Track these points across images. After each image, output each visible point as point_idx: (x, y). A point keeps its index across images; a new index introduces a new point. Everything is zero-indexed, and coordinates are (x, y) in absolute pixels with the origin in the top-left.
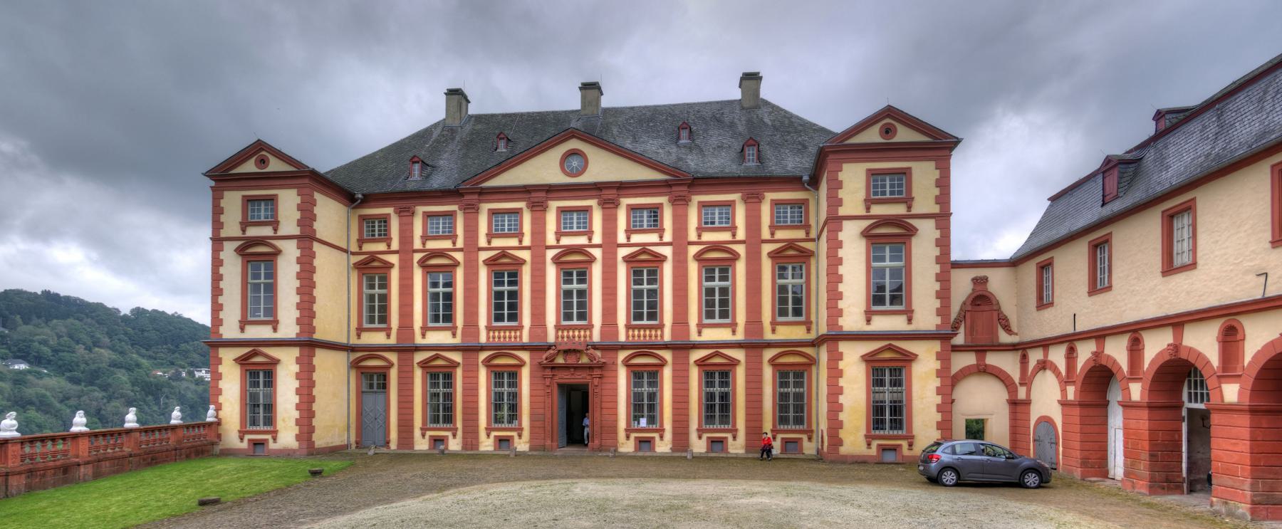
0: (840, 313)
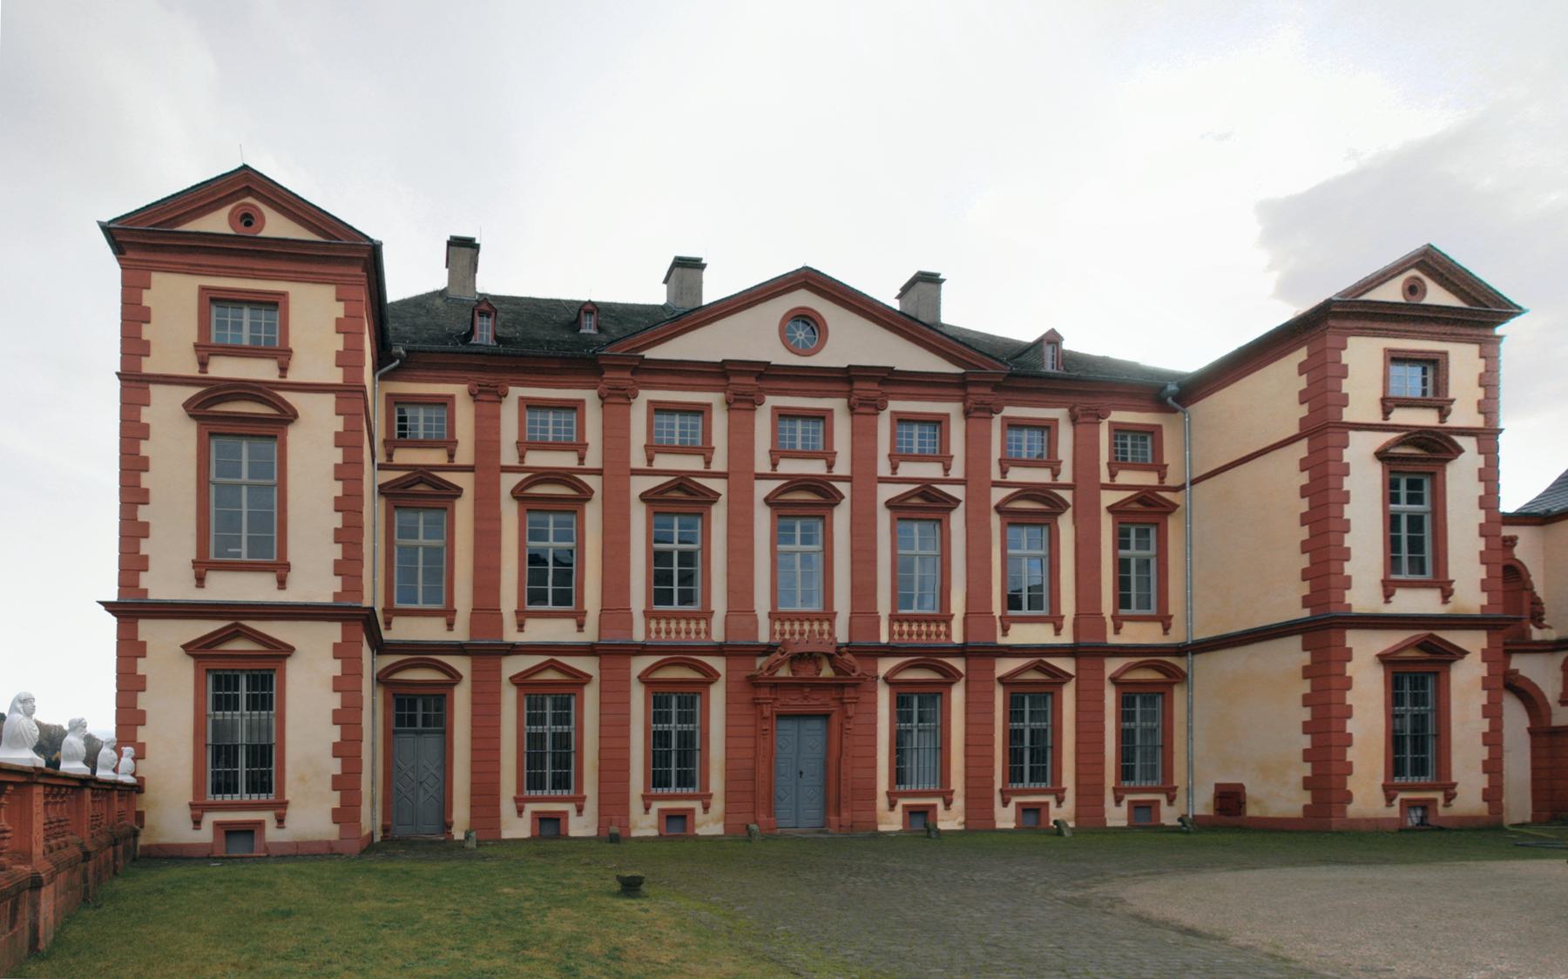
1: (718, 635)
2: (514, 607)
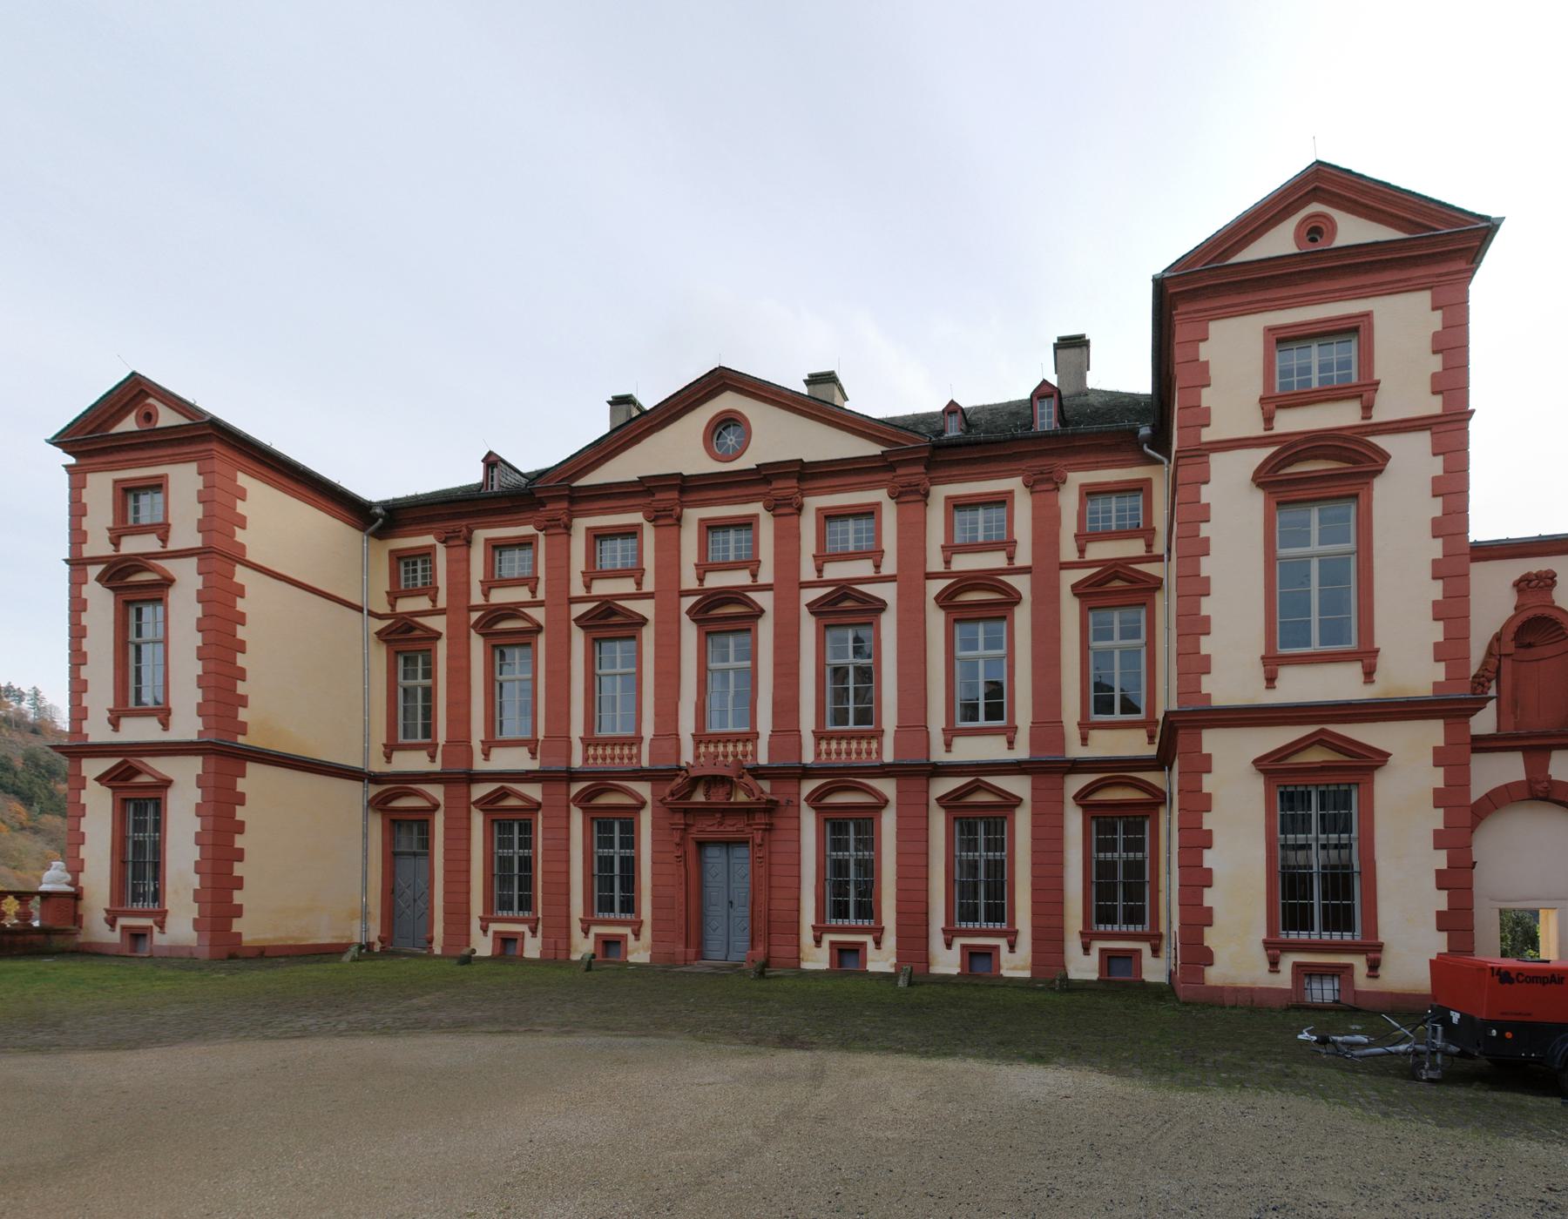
0: (1205, 665)
1: (888, 757)
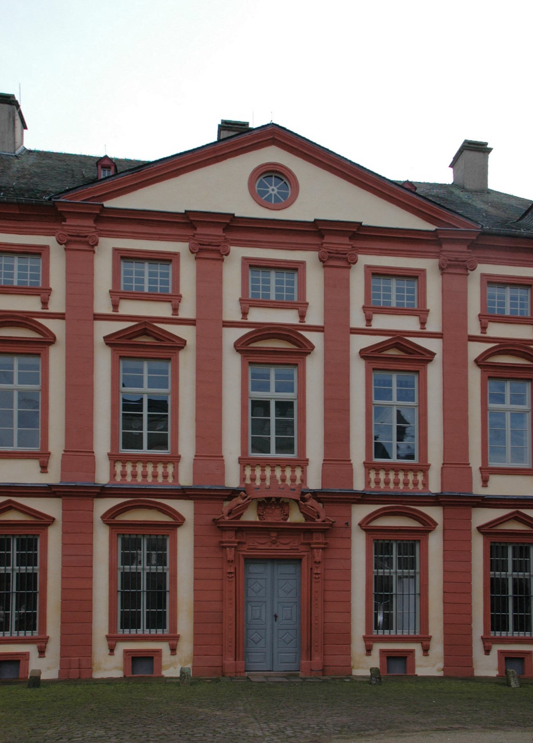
1: (435, 487)
2: (237, 454)
